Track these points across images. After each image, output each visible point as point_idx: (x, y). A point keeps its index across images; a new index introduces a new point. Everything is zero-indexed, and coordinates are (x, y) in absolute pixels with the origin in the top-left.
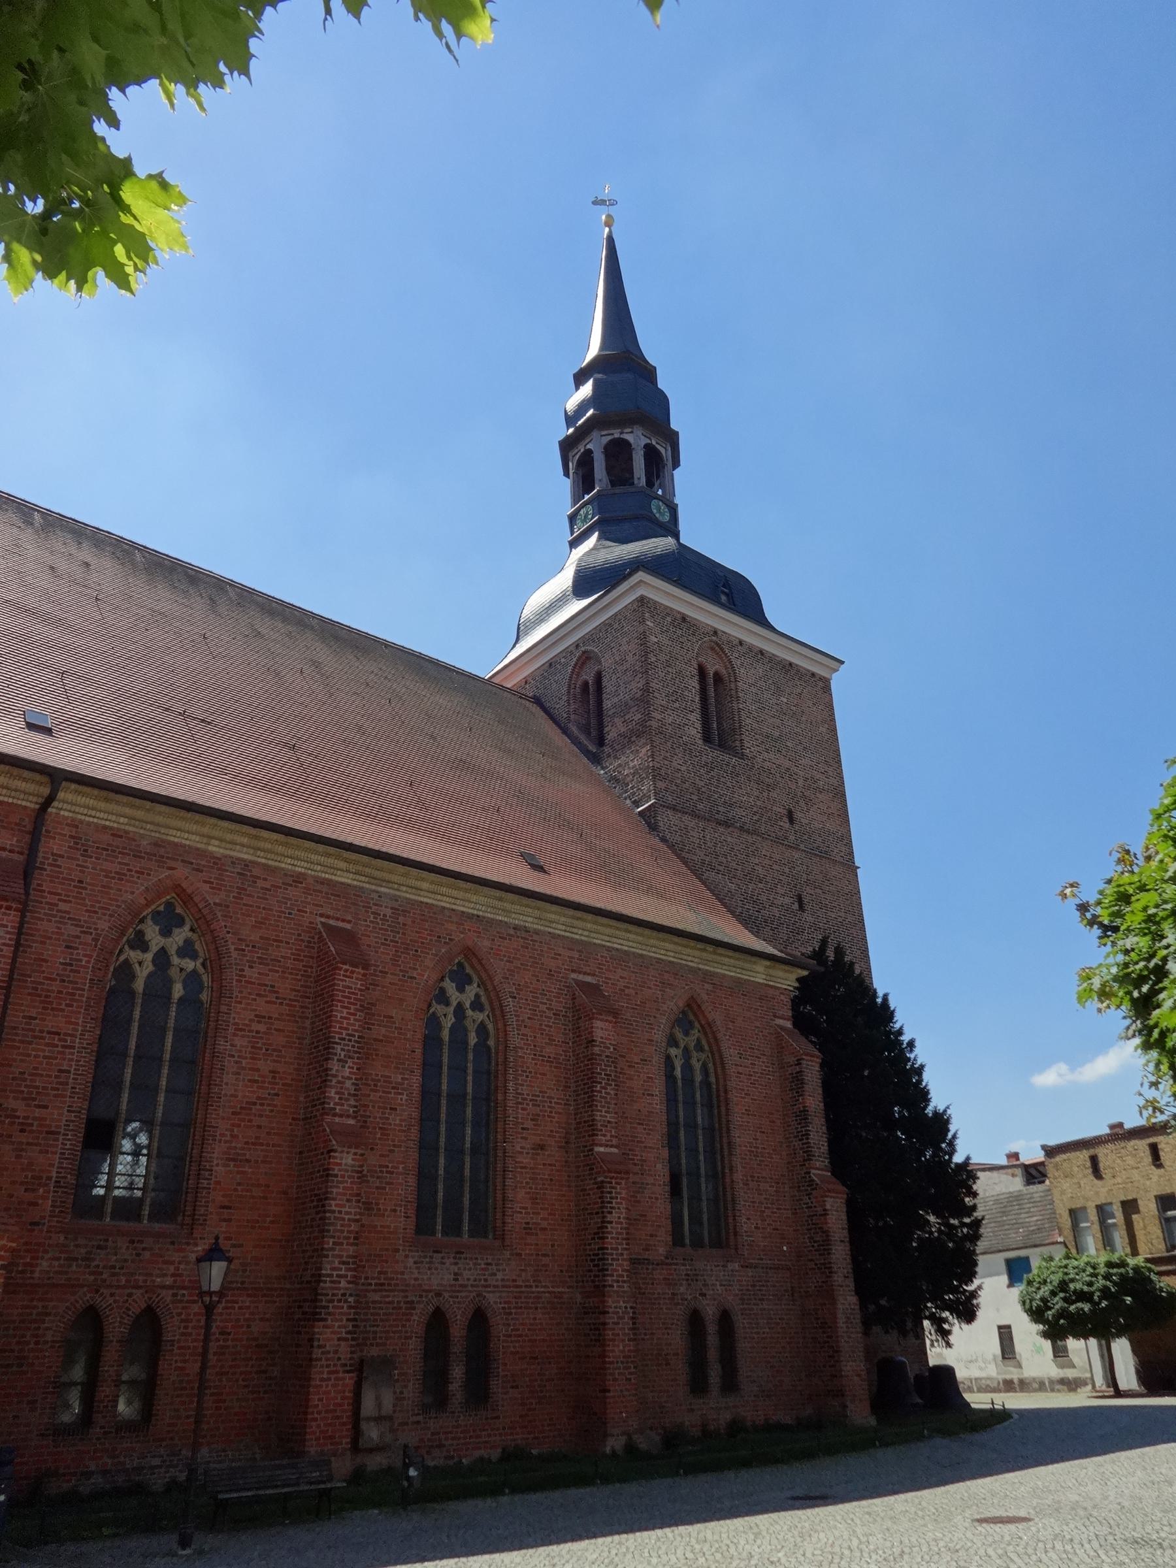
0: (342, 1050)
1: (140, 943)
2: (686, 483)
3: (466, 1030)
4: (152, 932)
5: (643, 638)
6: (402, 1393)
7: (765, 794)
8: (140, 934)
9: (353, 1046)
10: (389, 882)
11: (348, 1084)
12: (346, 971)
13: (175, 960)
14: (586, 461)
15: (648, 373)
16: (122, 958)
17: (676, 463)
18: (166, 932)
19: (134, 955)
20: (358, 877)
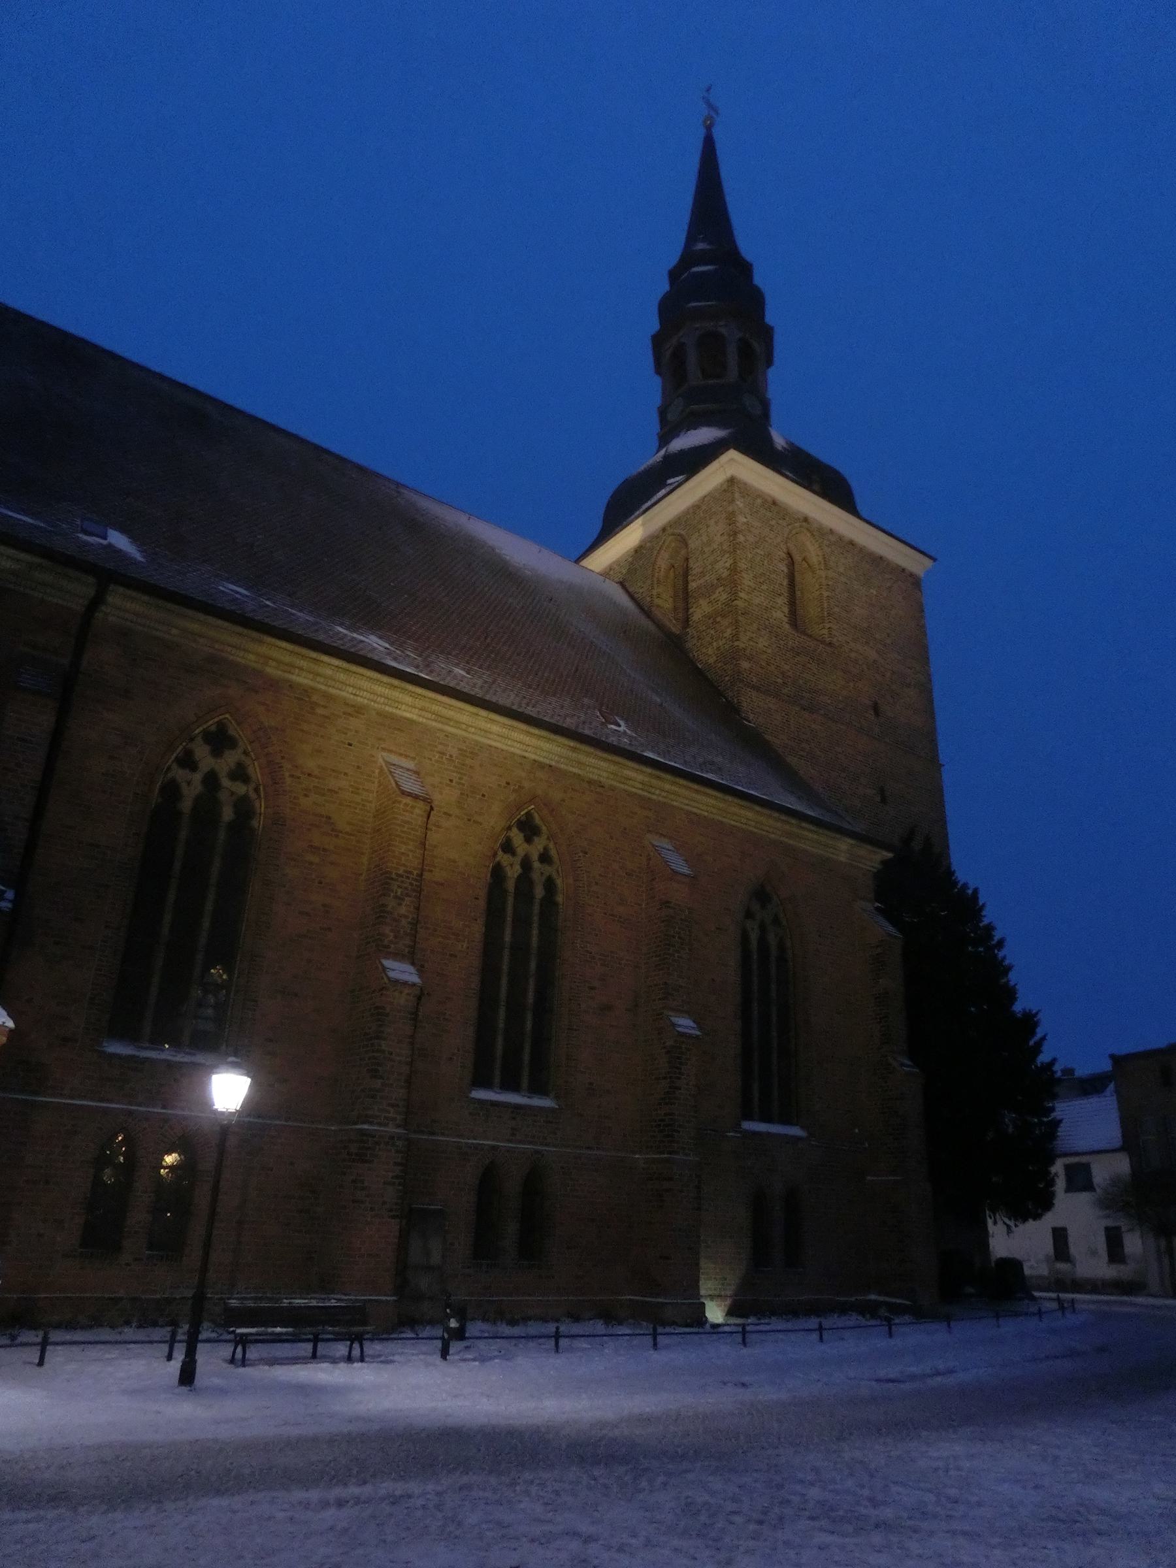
0: (399, 887)
1: (188, 762)
2: (780, 382)
3: (531, 883)
4: (201, 751)
5: (731, 518)
6: (452, 1244)
7: (851, 684)
8: (189, 753)
9: (411, 884)
10: (457, 722)
11: (404, 922)
12: (406, 805)
13: (226, 782)
14: (679, 355)
15: (746, 269)
16: (170, 775)
17: (769, 362)
18: (217, 752)
19: (180, 774)
20: (423, 713)
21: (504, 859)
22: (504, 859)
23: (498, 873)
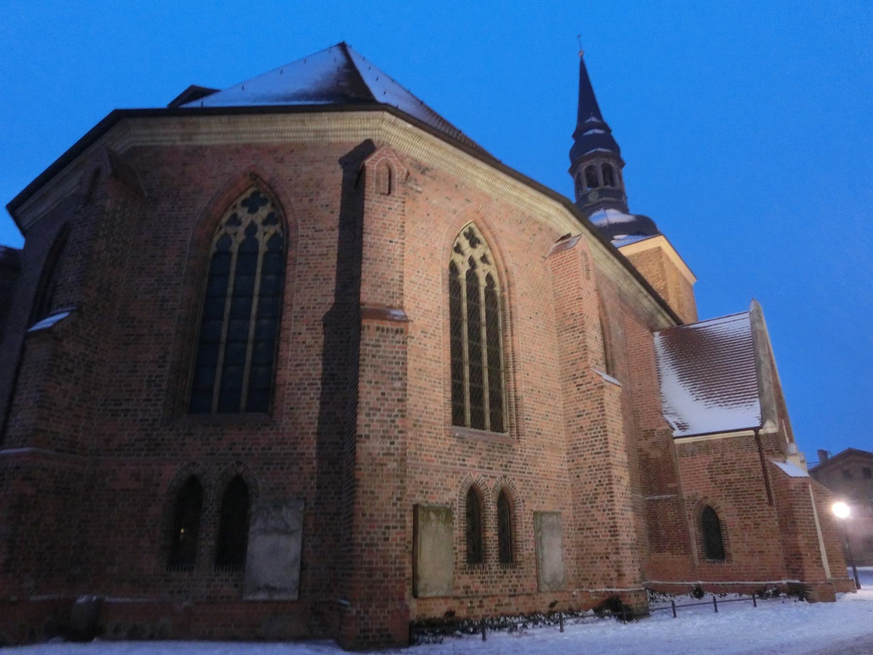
1: (235, 221)
21: (458, 258)
22: (458, 258)
23: (453, 268)
